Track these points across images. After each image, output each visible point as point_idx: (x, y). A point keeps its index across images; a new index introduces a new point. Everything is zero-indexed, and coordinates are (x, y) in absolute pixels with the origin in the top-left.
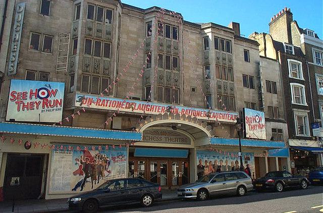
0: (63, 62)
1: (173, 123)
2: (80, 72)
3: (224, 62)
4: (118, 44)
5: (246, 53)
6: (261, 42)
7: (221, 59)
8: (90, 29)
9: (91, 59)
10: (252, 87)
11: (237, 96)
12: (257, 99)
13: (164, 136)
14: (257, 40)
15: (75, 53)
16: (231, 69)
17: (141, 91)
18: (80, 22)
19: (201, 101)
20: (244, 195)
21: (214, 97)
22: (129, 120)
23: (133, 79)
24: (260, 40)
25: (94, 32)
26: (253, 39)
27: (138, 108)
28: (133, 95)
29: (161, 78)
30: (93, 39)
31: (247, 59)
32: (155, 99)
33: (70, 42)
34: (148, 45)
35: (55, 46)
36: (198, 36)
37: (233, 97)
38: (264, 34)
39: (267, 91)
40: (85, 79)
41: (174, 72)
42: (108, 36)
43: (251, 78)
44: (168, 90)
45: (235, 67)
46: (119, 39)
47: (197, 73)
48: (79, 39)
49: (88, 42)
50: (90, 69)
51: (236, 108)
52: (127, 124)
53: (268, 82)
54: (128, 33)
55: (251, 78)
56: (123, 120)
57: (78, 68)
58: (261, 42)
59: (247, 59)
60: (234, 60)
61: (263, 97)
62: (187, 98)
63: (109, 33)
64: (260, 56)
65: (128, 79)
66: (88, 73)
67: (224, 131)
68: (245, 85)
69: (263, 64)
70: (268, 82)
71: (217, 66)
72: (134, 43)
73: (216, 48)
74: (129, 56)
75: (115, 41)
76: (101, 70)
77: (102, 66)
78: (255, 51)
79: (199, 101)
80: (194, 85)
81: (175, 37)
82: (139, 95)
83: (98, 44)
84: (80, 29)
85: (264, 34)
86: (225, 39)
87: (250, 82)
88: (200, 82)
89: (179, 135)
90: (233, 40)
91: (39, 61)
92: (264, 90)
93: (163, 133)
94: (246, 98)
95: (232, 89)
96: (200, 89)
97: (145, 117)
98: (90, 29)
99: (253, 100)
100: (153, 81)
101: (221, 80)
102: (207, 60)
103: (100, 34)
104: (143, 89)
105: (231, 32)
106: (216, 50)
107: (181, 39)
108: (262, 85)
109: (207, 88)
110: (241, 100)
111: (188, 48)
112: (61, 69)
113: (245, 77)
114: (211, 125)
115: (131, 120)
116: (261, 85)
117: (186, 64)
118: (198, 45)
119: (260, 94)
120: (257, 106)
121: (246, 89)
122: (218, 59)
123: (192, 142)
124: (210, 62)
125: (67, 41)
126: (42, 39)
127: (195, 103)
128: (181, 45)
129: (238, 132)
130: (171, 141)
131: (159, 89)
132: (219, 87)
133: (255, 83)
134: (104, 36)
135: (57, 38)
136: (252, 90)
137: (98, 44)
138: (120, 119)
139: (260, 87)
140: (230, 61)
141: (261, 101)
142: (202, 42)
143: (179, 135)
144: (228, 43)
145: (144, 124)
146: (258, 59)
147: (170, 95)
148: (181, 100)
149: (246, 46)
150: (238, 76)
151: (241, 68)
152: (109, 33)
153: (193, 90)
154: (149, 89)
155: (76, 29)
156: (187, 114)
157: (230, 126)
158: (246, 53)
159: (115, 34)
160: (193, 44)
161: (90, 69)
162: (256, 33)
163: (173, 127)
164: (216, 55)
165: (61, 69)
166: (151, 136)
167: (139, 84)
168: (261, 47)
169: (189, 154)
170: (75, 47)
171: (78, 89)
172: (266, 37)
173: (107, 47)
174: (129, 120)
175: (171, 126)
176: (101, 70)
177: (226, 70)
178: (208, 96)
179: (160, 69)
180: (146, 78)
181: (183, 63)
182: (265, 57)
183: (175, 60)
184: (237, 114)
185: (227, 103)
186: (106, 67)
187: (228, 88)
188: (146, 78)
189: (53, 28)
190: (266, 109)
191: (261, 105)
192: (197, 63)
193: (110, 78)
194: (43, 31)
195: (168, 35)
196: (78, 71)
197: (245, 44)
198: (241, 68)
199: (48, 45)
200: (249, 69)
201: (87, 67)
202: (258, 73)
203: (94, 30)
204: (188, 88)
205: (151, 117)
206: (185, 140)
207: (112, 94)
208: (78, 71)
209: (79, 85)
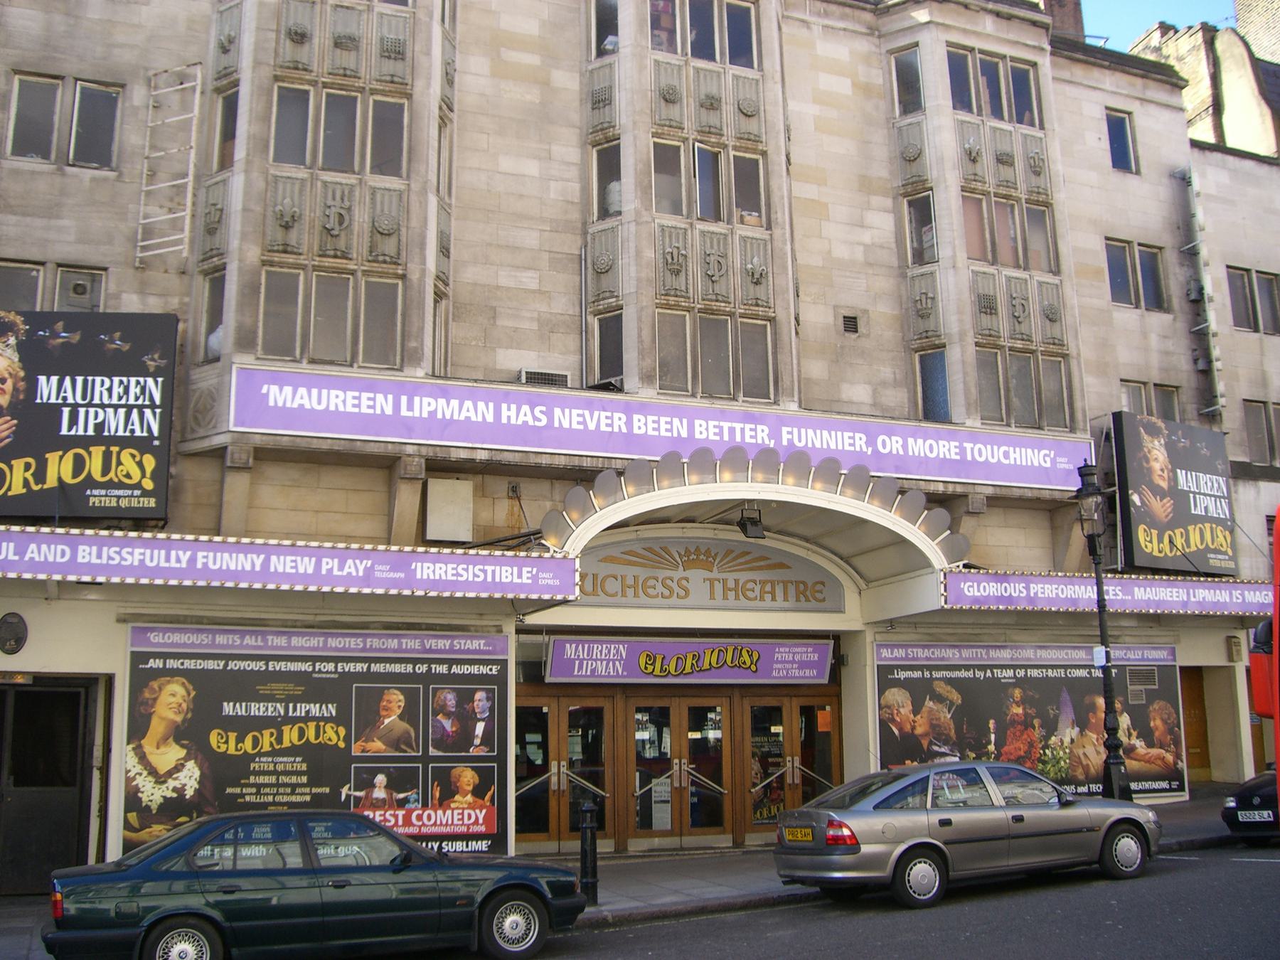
0: (171, 211)
1: (743, 502)
2: (254, 254)
3: (1006, 172)
4: (447, 104)
5: (1118, 129)
6: (1194, 68)
7: (987, 160)
8: (299, 37)
9: (309, 186)
10: (1157, 301)
11: (1083, 345)
12: (1182, 370)
13: (707, 574)
14: (1172, 62)
15: (226, 161)
16: (1040, 210)
17: (572, 341)
18: (238, 181)
19: (896, 384)
20: (1143, 871)
21: (960, 362)
22: (514, 493)
23: (529, 280)
24: (1186, 55)
25: (318, 54)
26: (1151, 57)
27: (578, 424)
28: (530, 361)
29: (673, 265)
30: (314, 83)
31: (1122, 154)
32: (647, 378)
33: (198, 110)
34: (600, 100)
35: (130, 134)
36: (864, 46)
37: (1059, 354)
38: (1210, 33)
39: (1238, 323)
40: (282, 291)
41: (741, 231)
42: (390, 67)
43: (1151, 257)
44: (711, 323)
45: (1063, 200)
46: (449, 80)
47: (867, 237)
48: (245, 92)
49: (293, 101)
50: (305, 238)
51: (1079, 415)
52: (500, 514)
53: (1238, 275)
54: (497, 43)
55: (1151, 257)
56: (480, 492)
57: (244, 236)
58: (1194, 68)
59: (1122, 154)
60: (1058, 165)
61: (1216, 353)
62: (816, 369)
63: (394, 52)
64: (1195, 144)
65: (505, 279)
66: (290, 259)
67: (1016, 542)
68: (1120, 290)
69: (1209, 178)
70: (1238, 275)
71: (971, 193)
72: (531, 95)
73: (961, 98)
74: (506, 164)
75: (429, 92)
76: (359, 242)
77: (361, 218)
78: (1166, 115)
79: (884, 384)
80: (853, 300)
81: (741, 51)
82: (562, 360)
83: (342, 108)
84: (247, 42)
85: (1210, 33)
86: (1003, 57)
87: (1140, 274)
88: (884, 283)
89: (781, 566)
90: (1045, 62)
91: (51, 211)
92: (1218, 316)
93: (698, 556)
94: (1127, 358)
95: (1052, 316)
96: (882, 315)
97: (581, 478)
98: (299, 37)
99: (1164, 370)
100: (634, 282)
101: (991, 270)
102: (914, 168)
103: (347, 59)
104: (584, 331)
105: (1034, 23)
106: (963, 116)
107: (771, 63)
108: (1208, 290)
109: (920, 309)
110: (1102, 369)
111: (811, 110)
112: (159, 246)
113: (1116, 250)
114: (945, 504)
115: (528, 487)
116: (1201, 290)
117: (804, 190)
118: (865, 90)
119: (1200, 339)
120: (1187, 401)
121: (1127, 317)
122: (972, 157)
123: (851, 600)
124: (932, 174)
125: (186, 107)
126: (67, 107)
127: (858, 393)
128: (773, 90)
129: (1091, 540)
130: (739, 595)
131: (669, 330)
132: (986, 306)
133: (1174, 279)
134: (369, 66)
135: (138, 95)
136: (1158, 320)
137: (342, 108)
138: (463, 488)
139: (1197, 302)
140: (1037, 168)
141: (1206, 373)
142: (883, 77)
143: (781, 563)
144: (1022, 80)
145: (587, 510)
146: (1185, 158)
147: (732, 351)
148: (785, 381)
149: (1113, 89)
150: (1082, 246)
151: (1095, 204)
152: (394, 52)
153: (851, 324)
154: (612, 329)
155: (231, 41)
156: (824, 447)
157: (1049, 510)
158: (1118, 129)
159: (428, 53)
160: (843, 86)
161: (305, 238)
162: (1165, 28)
163: (743, 525)
164: (962, 138)
165: (159, 246)
166: (630, 572)
167: (563, 305)
168: (1197, 95)
169: (839, 661)
170: (229, 134)
171: (245, 342)
172: (1219, 45)
173: (390, 124)
174: (514, 493)
175: (736, 516)
176: (359, 242)
177: (1020, 213)
178: (929, 362)
179: (670, 220)
180: (596, 271)
181: (779, 186)
182: (1220, 147)
183: (748, 175)
184: (1082, 448)
185: (1028, 386)
186: (384, 225)
187: (1034, 308)
188: (596, 271)
189: (122, 46)
190: (1232, 417)
191: (1207, 394)
192: (866, 185)
193: (403, 277)
194: (70, 66)
195: (703, 48)
196: (242, 253)
197: (1110, 80)
198: (1095, 204)
199: (96, 146)
200: (1139, 209)
201: (287, 227)
202: (1185, 227)
203: (320, 40)
204: (819, 316)
205: (620, 473)
206: (815, 591)
207: (410, 357)
208: (242, 253)
209: (248, 321)
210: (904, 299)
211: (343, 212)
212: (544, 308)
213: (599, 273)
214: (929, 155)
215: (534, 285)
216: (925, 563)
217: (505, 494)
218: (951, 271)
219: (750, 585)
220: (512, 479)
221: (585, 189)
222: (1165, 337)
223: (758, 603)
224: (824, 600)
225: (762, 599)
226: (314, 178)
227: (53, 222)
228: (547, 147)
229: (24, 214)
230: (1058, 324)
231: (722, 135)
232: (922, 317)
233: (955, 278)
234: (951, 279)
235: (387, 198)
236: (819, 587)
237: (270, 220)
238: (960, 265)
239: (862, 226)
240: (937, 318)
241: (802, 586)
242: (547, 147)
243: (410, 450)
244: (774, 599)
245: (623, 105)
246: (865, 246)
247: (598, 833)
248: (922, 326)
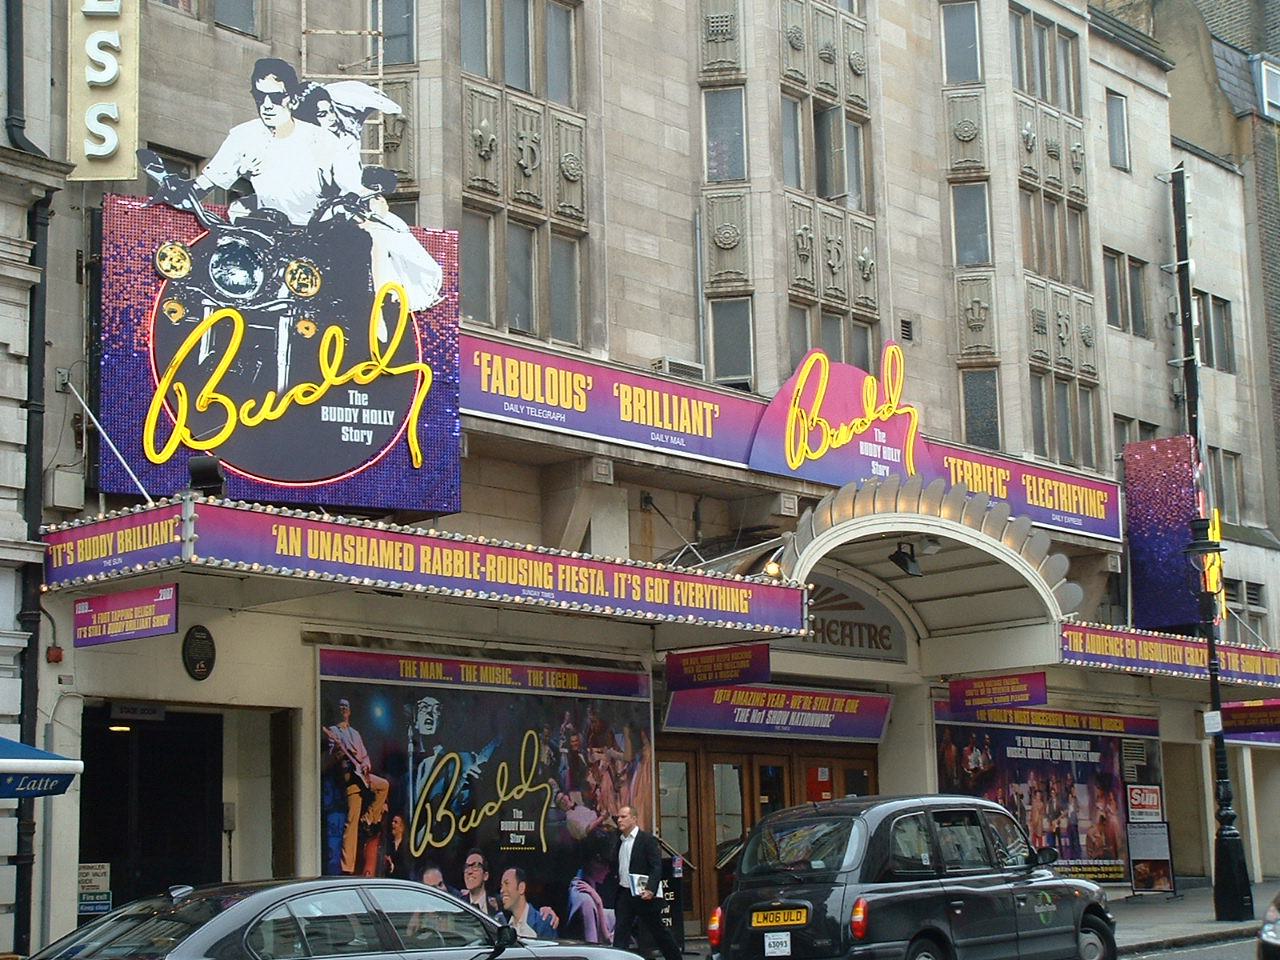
23: (649, 247)
79: (933, 403)
102: (969, 153)
210: (950, 304)
211: (534, 146)
212: (664, 284)
213: (721, 249)
214: (989, 138)
215: (653, 254)
216: (1044, 614)
217: (638, 505)
218: (1011, 279)
219: (834, 627)
220: (644, 488)
221: (695, 139)
222: (1148, 368)
223: (838, 648)
224: (889, 648)
225: (843, 644)
226: (504, 101)
227: (210, 104)
228: (659, 81)
229: (179, 88)
230: (1092, 349)
231: (835, 96)
232: (972, 328)
233: (1010, 291)
234: (1009, 289)
235: (528, 119)
236: (886, 632)
237: (469, 146)
238: (1018, 274)
239: (915, 214)
240: (991, 332)
241: (873, 630)
242: (659, 81)
243: (602, 449)
244: (852, 644)
245: (750, 45)
246: (919, 239)
247: (686, 913)
248: (972, 339)
